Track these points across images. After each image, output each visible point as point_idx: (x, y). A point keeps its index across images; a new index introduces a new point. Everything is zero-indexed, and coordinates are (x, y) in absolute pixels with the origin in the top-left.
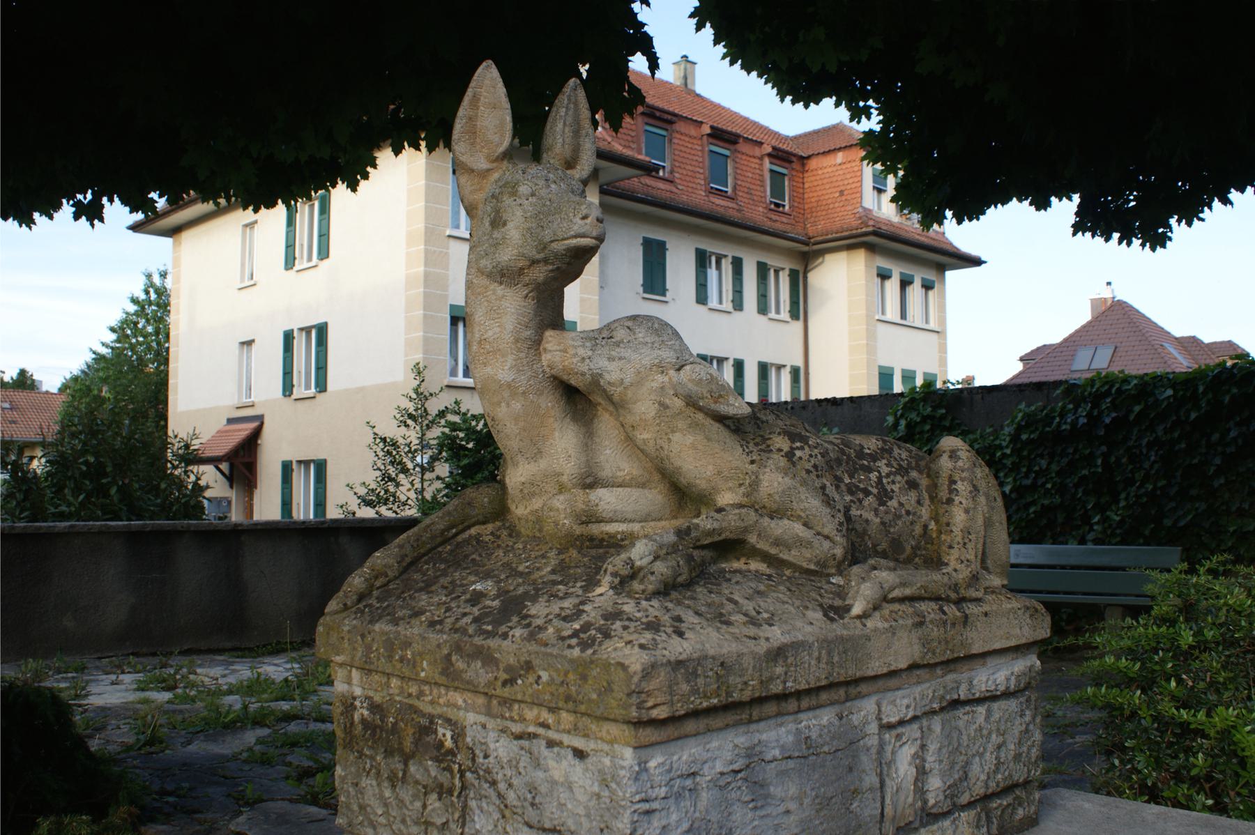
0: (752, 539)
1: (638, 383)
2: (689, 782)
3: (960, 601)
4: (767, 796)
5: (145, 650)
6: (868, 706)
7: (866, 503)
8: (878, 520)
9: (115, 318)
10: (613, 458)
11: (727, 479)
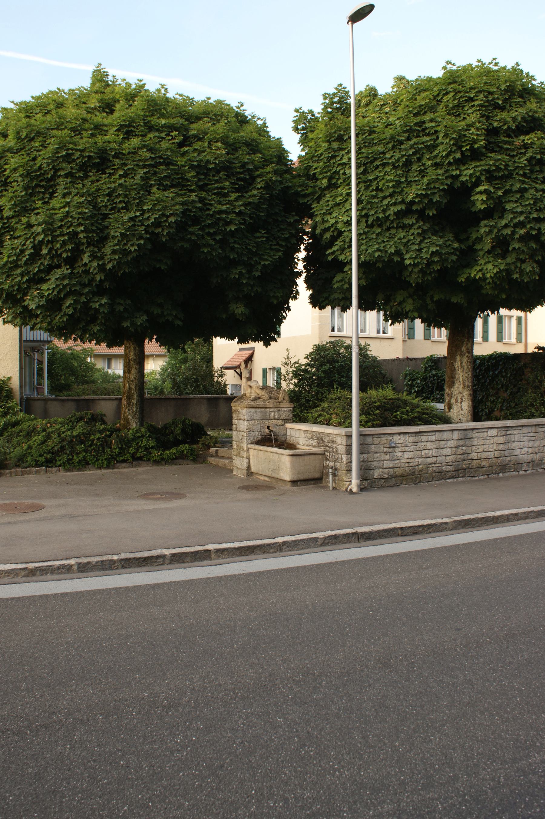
10: (253, 391)
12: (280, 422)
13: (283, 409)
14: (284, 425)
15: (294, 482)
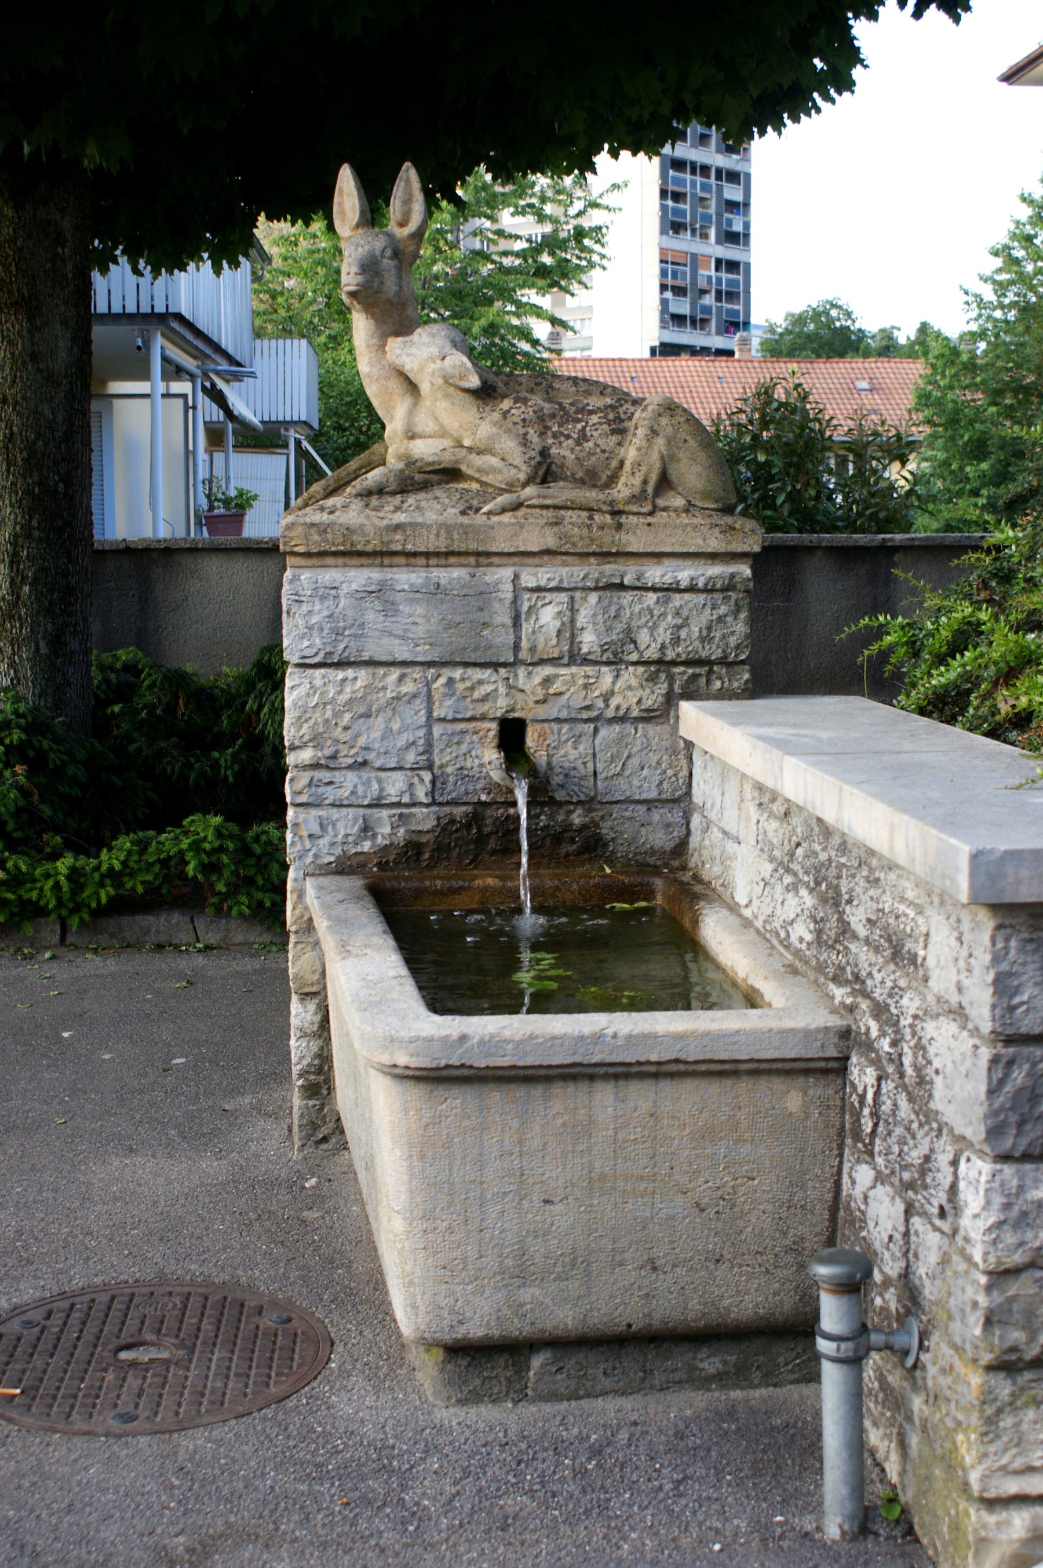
0: (463, 468)
1: (421, 370)
2: (333, 592)
3: (616, 513)
4: (397, 610)
6: (507, 573)
7: (565, 444)
9: (798, 309)
11: (466, 430)
12: (629, 689)
13: (655, 574)
14: (662, 713)
15: (482, 1360)
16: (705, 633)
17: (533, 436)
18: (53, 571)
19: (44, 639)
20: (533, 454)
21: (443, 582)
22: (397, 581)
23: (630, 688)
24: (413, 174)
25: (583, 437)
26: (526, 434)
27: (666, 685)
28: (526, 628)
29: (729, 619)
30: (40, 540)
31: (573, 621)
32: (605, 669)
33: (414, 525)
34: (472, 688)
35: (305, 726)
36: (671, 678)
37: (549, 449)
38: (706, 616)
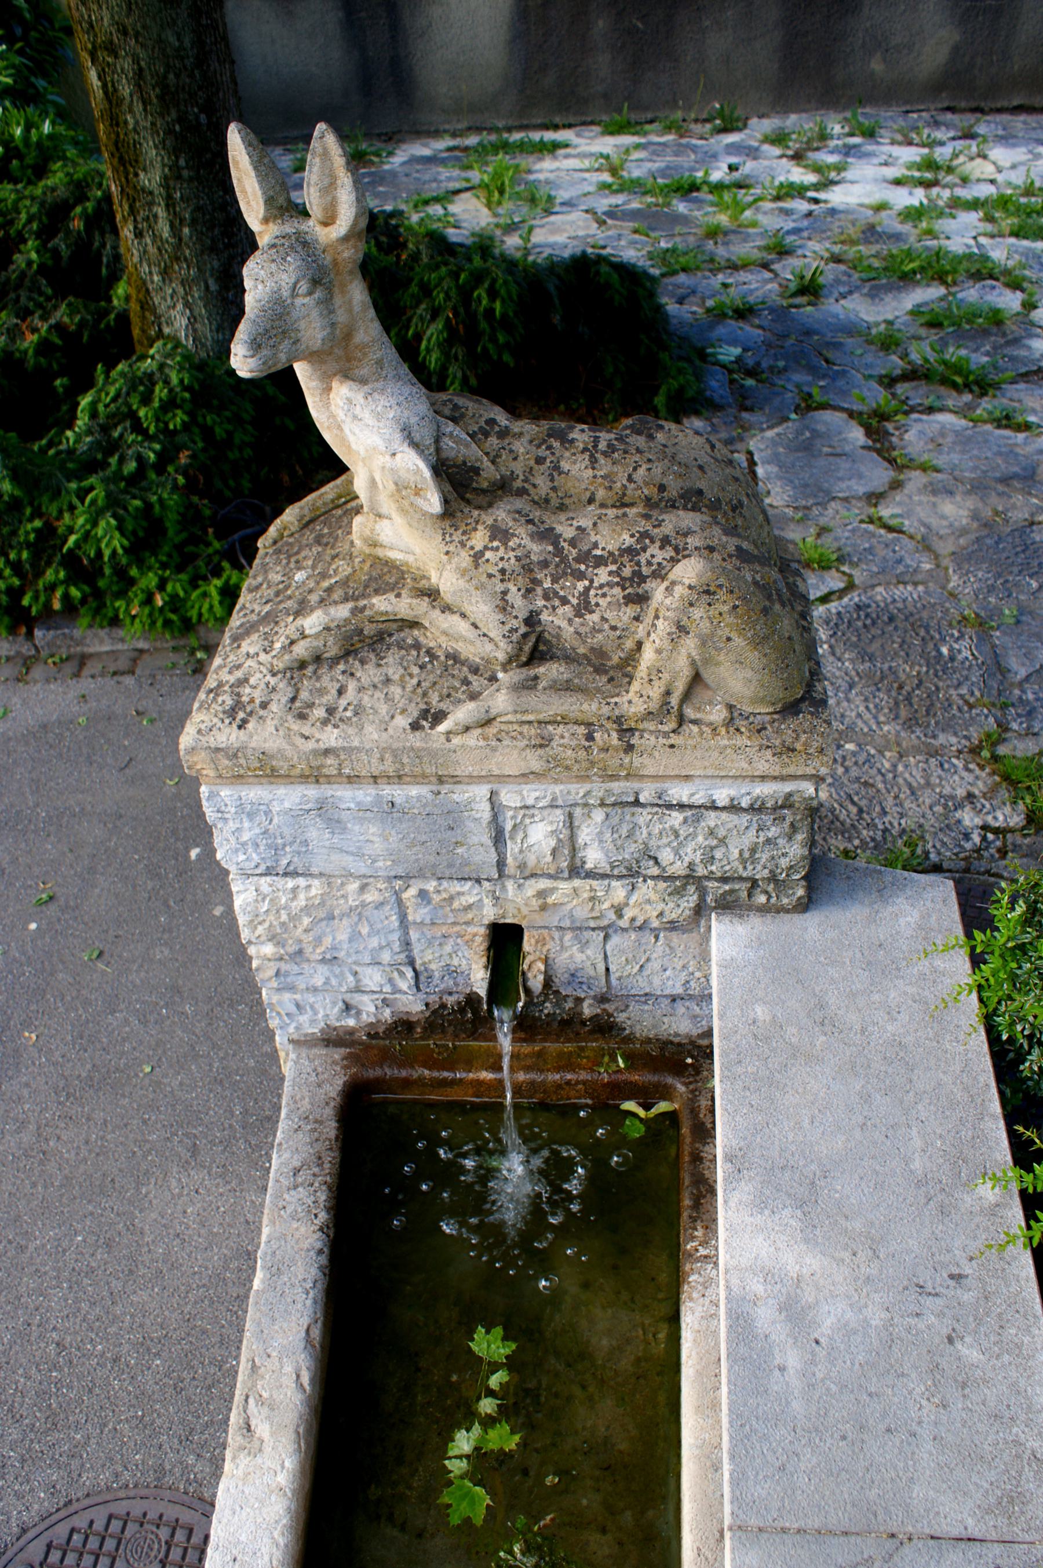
5: (963, 104)
7: (560, 611)
8: (572, 629)
16: (747, 855)
17: (515, 598)
18: (210, 208)
19: (212, 275)
20: (515, 623)
21: (398, 801)
22: (340, 799)
23: (649, 901)
24: (331, 140)
25: (584, 607)
26: (505, 593)
27: (695, 897)
28: (512, 848)
29: (781, 842)
30: (191, 180)
31: (572, 838)
32: (615, 883)
33: (350, 750)
34: (451, 898)
35: (260, 928)
36: (702, 892)
37: (538, 614)
38: (750, 838)
